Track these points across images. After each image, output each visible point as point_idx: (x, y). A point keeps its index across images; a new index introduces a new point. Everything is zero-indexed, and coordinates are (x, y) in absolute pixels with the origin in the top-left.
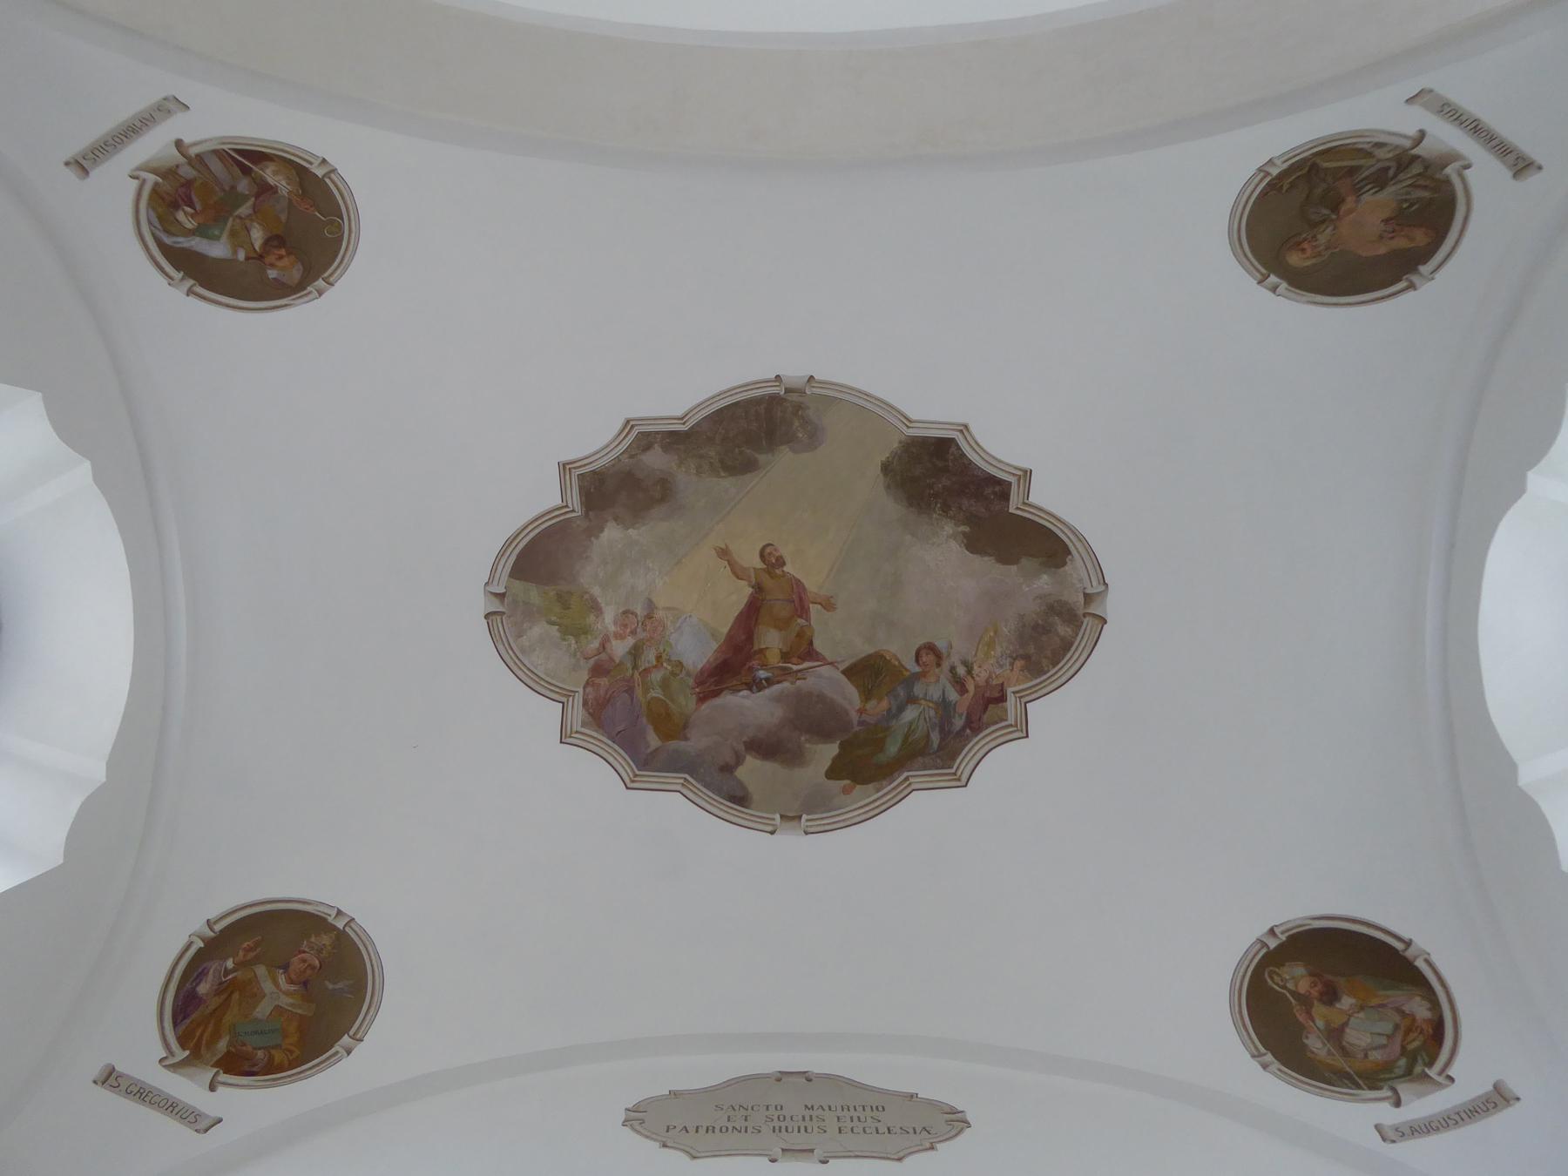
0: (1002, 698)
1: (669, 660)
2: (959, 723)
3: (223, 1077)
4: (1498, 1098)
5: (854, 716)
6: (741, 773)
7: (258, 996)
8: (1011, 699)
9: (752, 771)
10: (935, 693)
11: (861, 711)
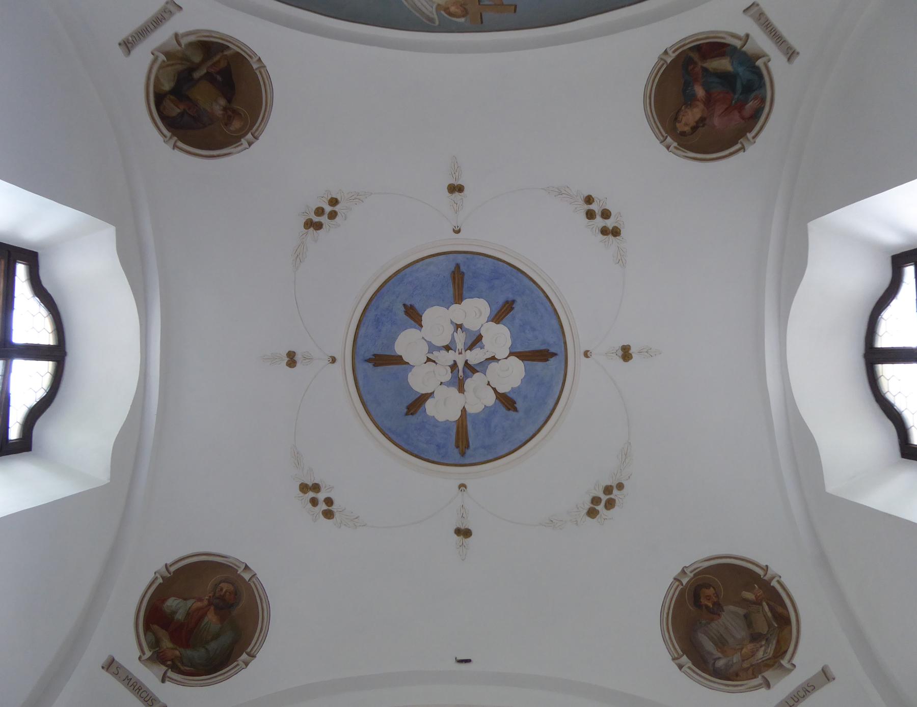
3: (170, 674)
4: (128, 45)
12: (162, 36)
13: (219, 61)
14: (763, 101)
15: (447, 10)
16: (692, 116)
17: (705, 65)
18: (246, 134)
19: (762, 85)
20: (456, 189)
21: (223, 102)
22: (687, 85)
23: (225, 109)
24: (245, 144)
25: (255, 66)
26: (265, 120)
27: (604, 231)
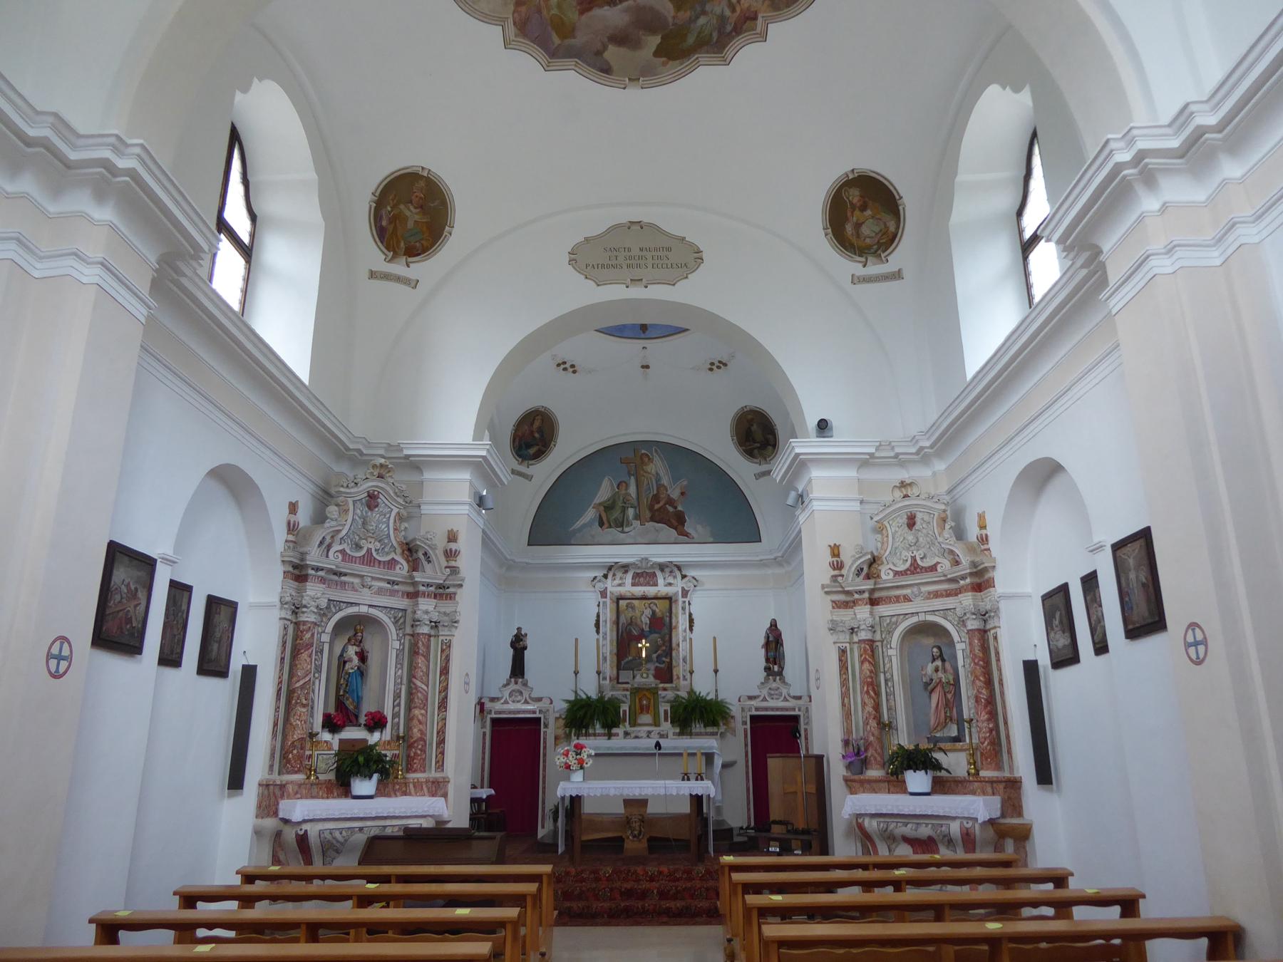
0: (755, 18)
1: (603, 594)
2: (729, 28)
3: (410, 259)
4: (897, 275)
5: (670, 20)
6: (607, 55)
7: (406, 219)
8: (760, 20)
9: (613, 54)
10: (718, 10)
11: (674, 17)
16: (537, 424)
22: (542, 436)
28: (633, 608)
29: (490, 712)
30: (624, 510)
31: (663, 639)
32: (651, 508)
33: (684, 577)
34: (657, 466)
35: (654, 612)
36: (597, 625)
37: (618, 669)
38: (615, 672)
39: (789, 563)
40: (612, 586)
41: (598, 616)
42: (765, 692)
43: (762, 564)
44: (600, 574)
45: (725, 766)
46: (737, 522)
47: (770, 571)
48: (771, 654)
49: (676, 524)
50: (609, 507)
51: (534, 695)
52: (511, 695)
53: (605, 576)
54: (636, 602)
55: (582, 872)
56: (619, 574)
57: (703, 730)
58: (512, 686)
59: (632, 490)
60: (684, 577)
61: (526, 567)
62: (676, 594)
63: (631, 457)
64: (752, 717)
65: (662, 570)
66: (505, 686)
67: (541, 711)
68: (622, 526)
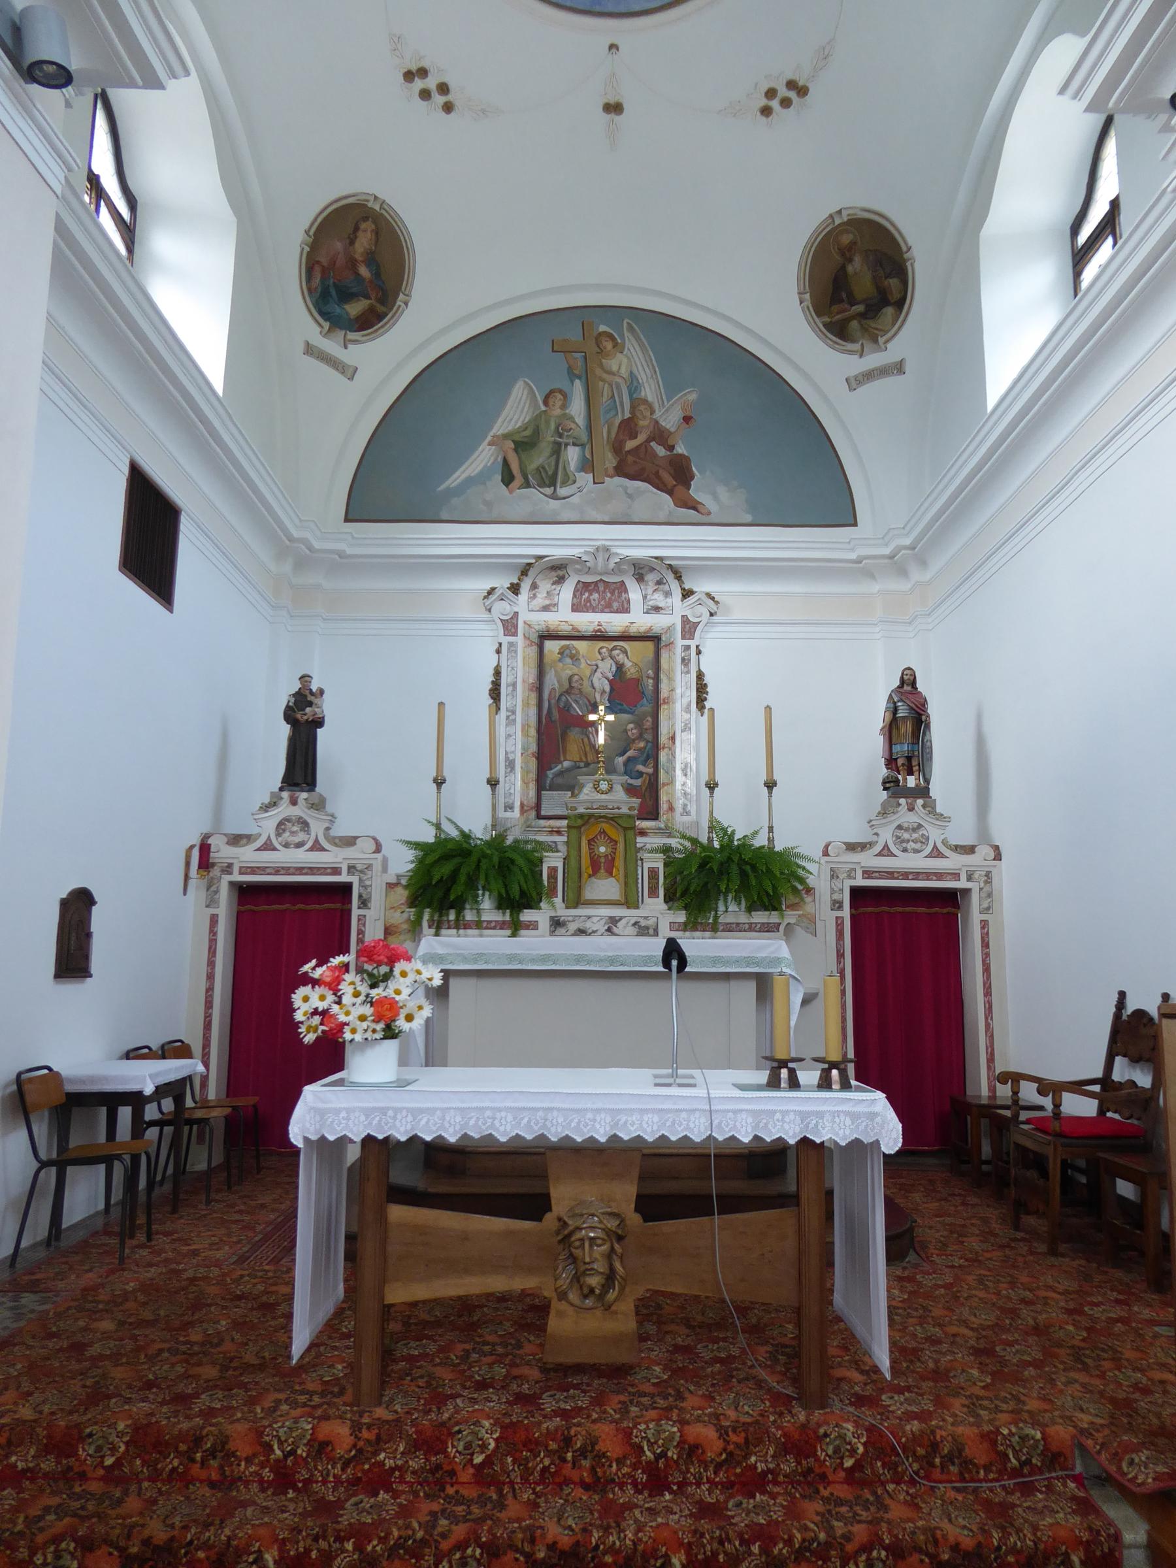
1: (510, 626)
4: (898, 368)
12: (874, 360)
13: (838, 313)
14: (310, 291)
15: (616, 345)
16: (363, 242)
17: (368, 302)
18: (839, 225)
19: (317, 305)
20: (614, 108)
21: (850, 269)
22: (377, 274)
23: (850, 260)
24: (844, 213)
25: (807, 296)
26: (816, 233)
27: (423, 72)
28: (575, 658)
29: (228, 869)
30: (557, 450)
31: (639, 724)
32: (617, 448)
33: (687, 594)
34: (632, 361)
35: (620, 667)
36: (495, 692)
37: (540, 787)
38: (532, 793)
39: (923, 563)
40: (530, 612)
41: (497, 673)
42: (886, 835)
43: (862, 569)
44: (502, 582)
45: (806, 1002)
46: (805, 480)
47: (876, 587)
48: (902, 749)
49: (670, 481)
50: (524, 443)
51: (339, 831)
52: (280, 827)
53: (515, 589)
54: (581, 646)
55: (385, 1434)
56: (545, 586)
57: (743, 918)
58: (284, 810)
59: (577, 408)
60: (687, 594)
61: (341, 564)
62: (669, 629)
63: (578, 337)
64: (856, 892)
65: (640, 578)
66: (266, 808)
67: (351, 869)
68: (553, 483)
